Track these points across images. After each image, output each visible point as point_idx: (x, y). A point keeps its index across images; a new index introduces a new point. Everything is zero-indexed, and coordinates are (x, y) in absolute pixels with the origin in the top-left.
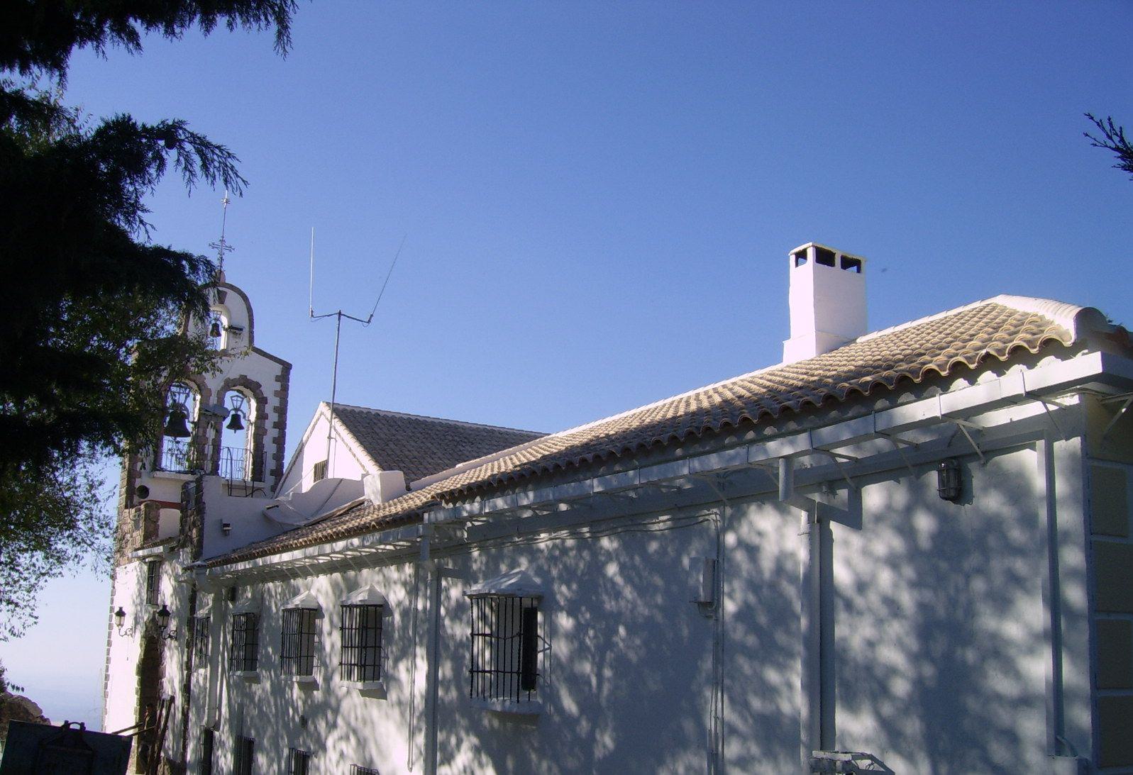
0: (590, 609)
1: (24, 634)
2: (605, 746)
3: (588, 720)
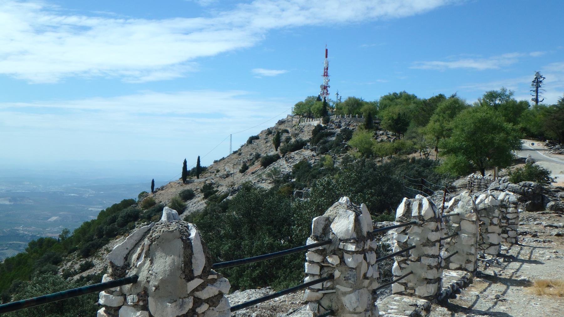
0: (487, 156)
1: (345, 277)
2: (498, 195)
3: (97, 299)
